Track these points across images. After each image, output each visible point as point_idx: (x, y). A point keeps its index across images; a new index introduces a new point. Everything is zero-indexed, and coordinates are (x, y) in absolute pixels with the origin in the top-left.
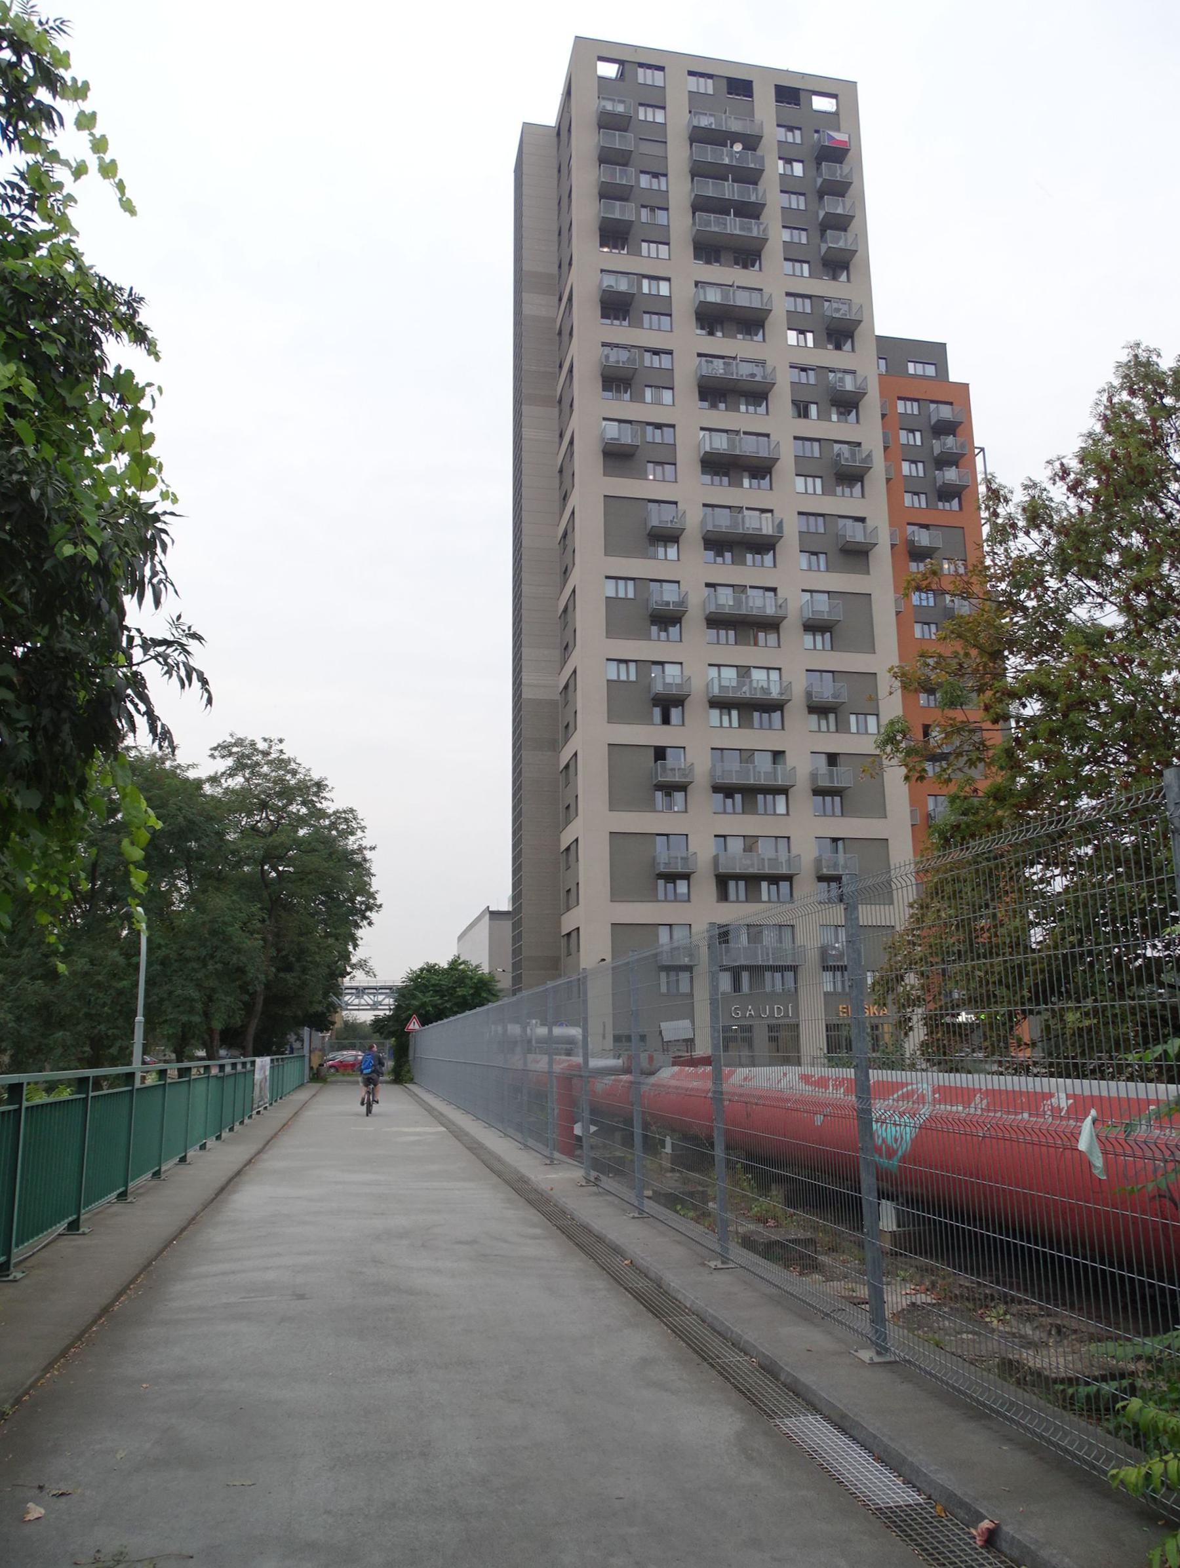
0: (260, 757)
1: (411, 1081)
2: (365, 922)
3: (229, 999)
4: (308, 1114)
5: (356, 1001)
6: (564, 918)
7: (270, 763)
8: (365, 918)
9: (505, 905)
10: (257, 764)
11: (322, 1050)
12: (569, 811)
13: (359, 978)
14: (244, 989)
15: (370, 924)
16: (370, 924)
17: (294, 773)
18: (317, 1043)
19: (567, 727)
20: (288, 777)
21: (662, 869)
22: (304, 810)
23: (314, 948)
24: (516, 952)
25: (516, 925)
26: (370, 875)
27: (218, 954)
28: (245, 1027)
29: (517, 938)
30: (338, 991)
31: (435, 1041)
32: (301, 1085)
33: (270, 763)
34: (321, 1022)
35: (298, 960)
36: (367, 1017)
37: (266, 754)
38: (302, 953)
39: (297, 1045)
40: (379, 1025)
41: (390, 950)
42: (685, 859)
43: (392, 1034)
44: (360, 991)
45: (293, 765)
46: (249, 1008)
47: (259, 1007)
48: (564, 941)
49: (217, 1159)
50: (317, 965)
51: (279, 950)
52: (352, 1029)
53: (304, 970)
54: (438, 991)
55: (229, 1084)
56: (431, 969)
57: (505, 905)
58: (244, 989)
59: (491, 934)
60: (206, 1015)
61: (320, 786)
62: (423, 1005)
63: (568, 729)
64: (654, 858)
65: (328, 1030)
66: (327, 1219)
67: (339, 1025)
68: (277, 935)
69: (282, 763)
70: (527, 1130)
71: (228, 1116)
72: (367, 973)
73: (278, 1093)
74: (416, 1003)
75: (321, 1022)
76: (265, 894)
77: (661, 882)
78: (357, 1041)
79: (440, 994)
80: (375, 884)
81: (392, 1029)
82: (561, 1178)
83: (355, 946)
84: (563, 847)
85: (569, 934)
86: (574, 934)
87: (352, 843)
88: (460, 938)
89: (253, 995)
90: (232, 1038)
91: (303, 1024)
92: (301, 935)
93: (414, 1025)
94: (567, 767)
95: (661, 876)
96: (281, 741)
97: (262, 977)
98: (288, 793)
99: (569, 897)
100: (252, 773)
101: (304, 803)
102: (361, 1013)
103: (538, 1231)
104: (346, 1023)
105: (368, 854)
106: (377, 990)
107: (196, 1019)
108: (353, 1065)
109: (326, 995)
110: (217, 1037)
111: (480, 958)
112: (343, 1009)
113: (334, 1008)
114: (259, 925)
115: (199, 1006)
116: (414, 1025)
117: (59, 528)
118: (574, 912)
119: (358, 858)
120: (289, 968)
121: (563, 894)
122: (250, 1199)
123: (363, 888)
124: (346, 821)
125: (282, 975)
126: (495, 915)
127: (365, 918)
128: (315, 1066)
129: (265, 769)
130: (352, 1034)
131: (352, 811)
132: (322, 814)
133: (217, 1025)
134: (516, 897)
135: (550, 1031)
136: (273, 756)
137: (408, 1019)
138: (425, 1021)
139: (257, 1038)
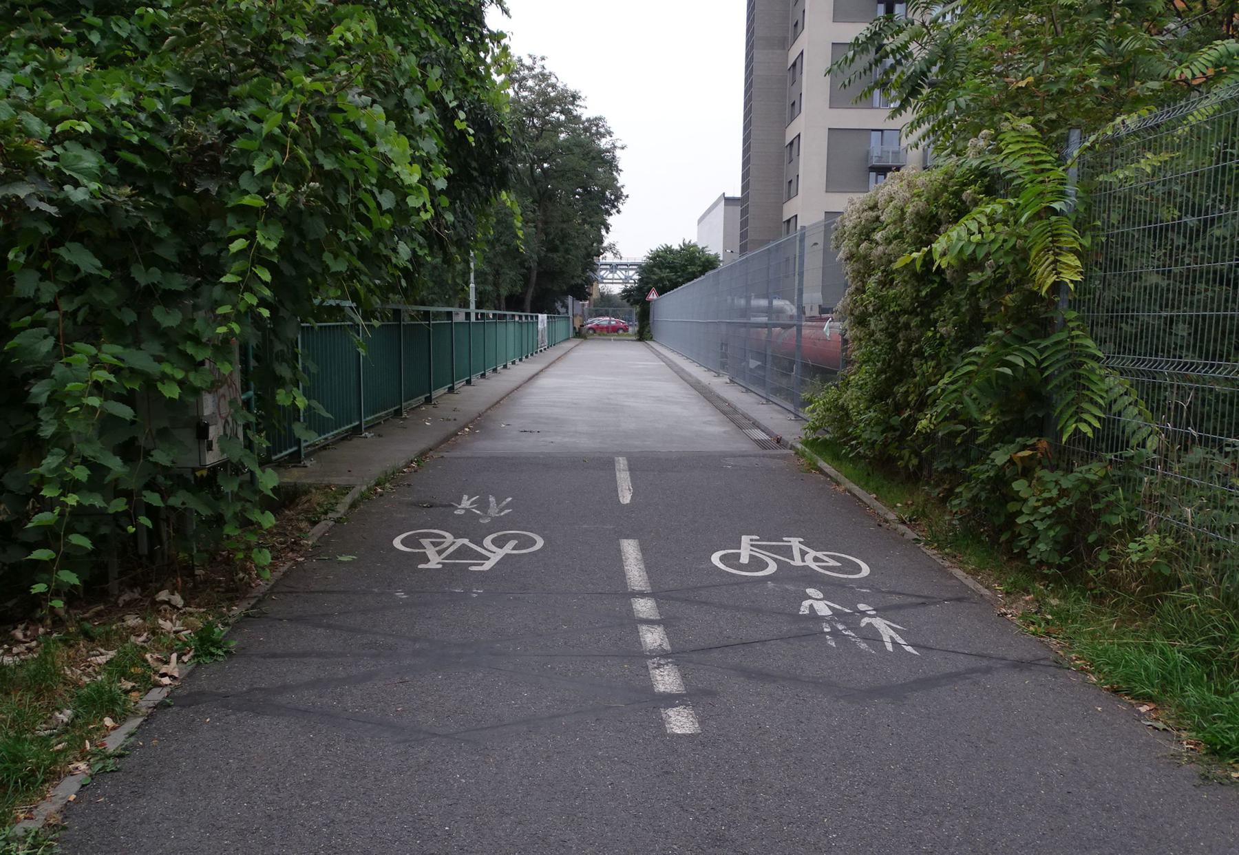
0: (526, 72)
1: (651, 339)
2: (614, 211)
3: (512, 273)
4: (574, 354)
5: (610, 276)
6: (785, 207)
7: (534, 77)
8: (615, 207)
9: (737, 193)
10: (524, 78)
11: (583, 315)
12: (794, 108)
13: (609, 257)
14: (522, 264)
15: (618, 212)
16: (618, 212)
17: (554, 86)
18: (578, 310)
19: (796, 25)
20: (550, 89)
21: (875, 162)
22: (563, 118)
23: (574, 234)
24: (743, 236)
25: (744, 212)
26: (618, 170)
27: (503, 239)
28: (524, 293)
29: (744, 224)
30: (593, 267)
31: (670, 307)
32: (568, 339)
33: (534, 77)
34: (581, 292)
35: (562, 243)
36: (616, 289)
37: (531, 69)
38: (564, 237)
39: (562, 310)
40: (627, 294)
41: (632, 235)
42: (896, 153)
43: (636, 302)
44: (613, 268)
45: (553, 80)
46: (526, 279)
47: (534, 278)
48: (784, 227)
49: (522, 370)
50: (577, 247)
51: (547, 234)
52: (606, 299)
53: (567, 251)
54: (672, 268)
55: (525, 327)
56: (668, 250)
57: (737, 193)
58: (522, 264)
59: (725, 218)
60: (496, 285)
61: (575, 97)
62: (661, 280)
63: (797, 27)
64: (868, 152)
65: (586, 299)
66: (586, 391)
67: (595, 296)
68: (546, 223)
69: (544, 77)
70: (740, 377)
71: (527, 350)
72: (615, 254)
73: (552, 344)
74: (656, 277)
75: (581, 292)
76: (535, 189)
77: (873, 175)
78: (610, 310)
79: (673, 269)
80: (622, 179)
81: (637, 298)
82: (719, 384)
83: (608, 230)
84: (788, 142)
85: (789, 221)
86: (793, 221)
87: (604, 143)
88: (700, 221)
89: (529, 269)
90: (514, 303)
91: (566, 294)
92: (563, 222)
93: (653, 296)
94: (794, 65)
95: (873, 169)
96: (543, 59)
97: (535, 257)
98: (548, 103)
99: (790, 187)
100: (520, 87)
101: (561, 112)
102: (613, 285)
103: (710, 418)
104: (602, 295)
105: (618, 153)
106: (628, 266)
107: (489, 288)
108: (607, 328)
109: (584, 271)
110: (503, 302)
111: (714, 244)
112: (599, 282)
113: (590, 282)
114: (532, 215)
115: (491, 278)
116: (653, 296)
117: (498, 131)
118: (794, 201)
119: (608, 156)
120: (554, 249)
121: (785, 185)
122: (544, 382)
123: (611, 183)
124: (595, 128)
125: (550, 255)
126: (729, 201)
127: (615, 207)
128: (577, 327)
129: (530, 83)
130: (606, 302)
131: (600, 119)
132: (577, 119)
133: (504, 292)
134: (745, 187)
135: (771, 303)
136: (537, 70)
137: (649, 291)
138: (661, 291)
139: (533, 303)
